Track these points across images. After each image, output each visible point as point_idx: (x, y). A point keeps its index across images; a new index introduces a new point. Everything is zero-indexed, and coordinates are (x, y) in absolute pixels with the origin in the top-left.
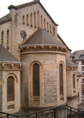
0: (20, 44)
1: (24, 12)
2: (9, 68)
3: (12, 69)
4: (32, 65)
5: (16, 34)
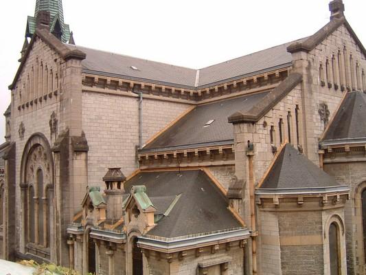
0: (319, 136)
1: (321, 54)
2: (294, 206)
3: (336, 206)
4: (360, 190)
5: (312, 114)
